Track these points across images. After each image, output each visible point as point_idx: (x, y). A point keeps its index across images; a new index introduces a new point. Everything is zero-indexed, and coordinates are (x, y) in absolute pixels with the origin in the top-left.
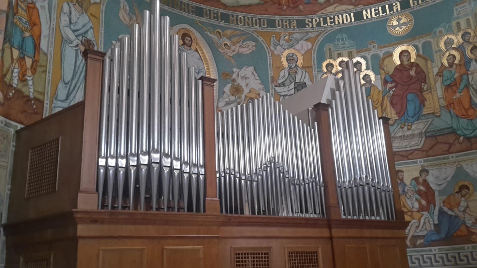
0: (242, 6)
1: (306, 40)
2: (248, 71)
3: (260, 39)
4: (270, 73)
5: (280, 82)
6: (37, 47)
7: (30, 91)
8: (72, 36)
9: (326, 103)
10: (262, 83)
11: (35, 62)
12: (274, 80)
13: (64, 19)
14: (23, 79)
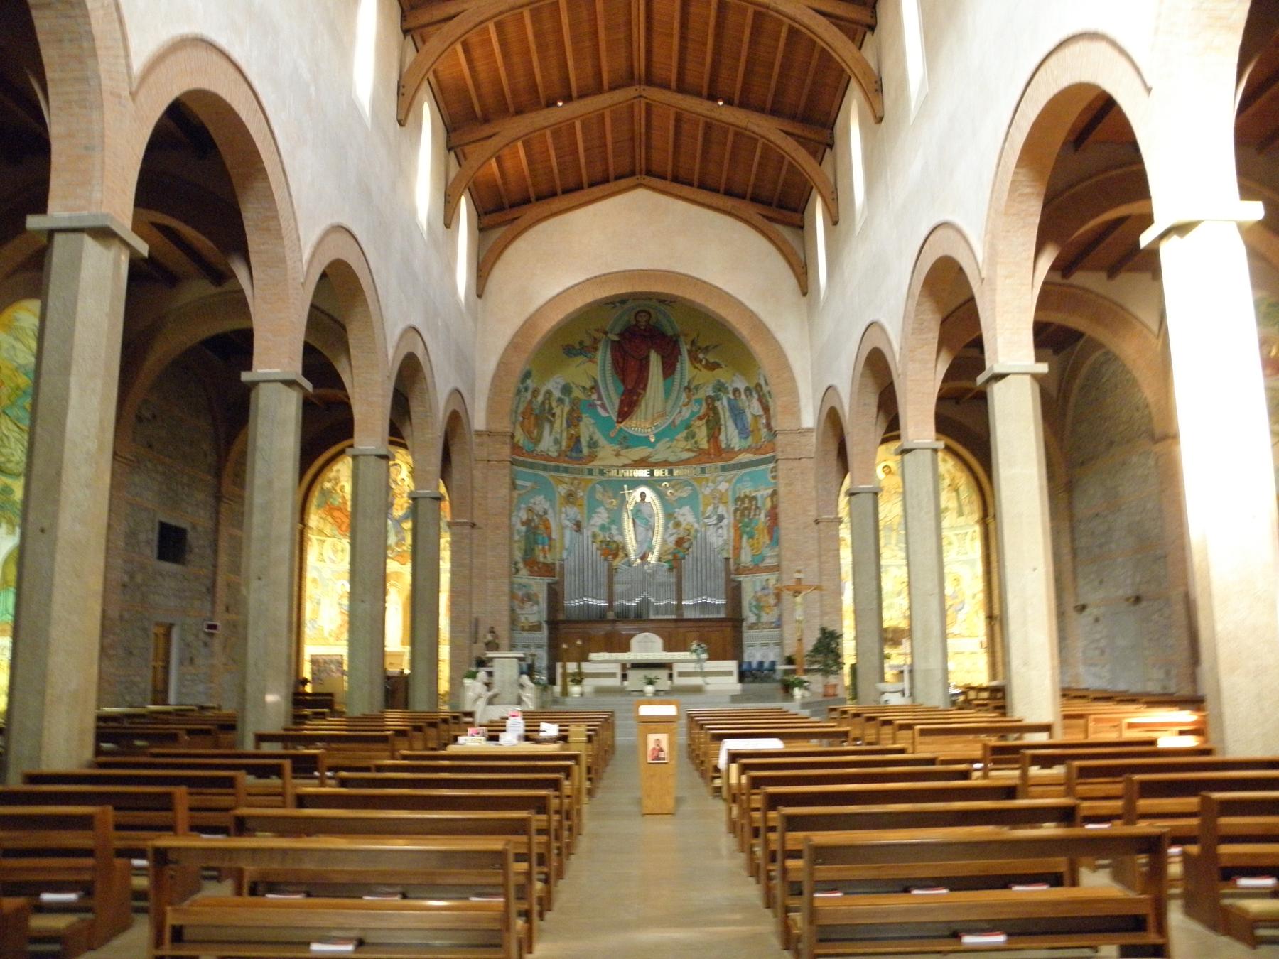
0: (683, 461)
1: (726, 482)
2: (686, 509)
3: (695, 484)
4: (701, 509)
5: (707, 514)
6: (550, 539)
7: (549, 560)
8: (567, 523)
9: (147, 926)
10: (696, 517)
11: (550, 546)
12: (703, 513)
13: (563, 515)
14: (545, 557)
